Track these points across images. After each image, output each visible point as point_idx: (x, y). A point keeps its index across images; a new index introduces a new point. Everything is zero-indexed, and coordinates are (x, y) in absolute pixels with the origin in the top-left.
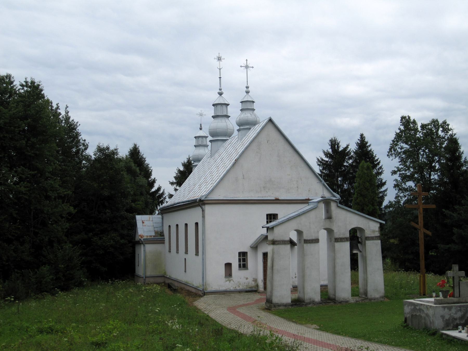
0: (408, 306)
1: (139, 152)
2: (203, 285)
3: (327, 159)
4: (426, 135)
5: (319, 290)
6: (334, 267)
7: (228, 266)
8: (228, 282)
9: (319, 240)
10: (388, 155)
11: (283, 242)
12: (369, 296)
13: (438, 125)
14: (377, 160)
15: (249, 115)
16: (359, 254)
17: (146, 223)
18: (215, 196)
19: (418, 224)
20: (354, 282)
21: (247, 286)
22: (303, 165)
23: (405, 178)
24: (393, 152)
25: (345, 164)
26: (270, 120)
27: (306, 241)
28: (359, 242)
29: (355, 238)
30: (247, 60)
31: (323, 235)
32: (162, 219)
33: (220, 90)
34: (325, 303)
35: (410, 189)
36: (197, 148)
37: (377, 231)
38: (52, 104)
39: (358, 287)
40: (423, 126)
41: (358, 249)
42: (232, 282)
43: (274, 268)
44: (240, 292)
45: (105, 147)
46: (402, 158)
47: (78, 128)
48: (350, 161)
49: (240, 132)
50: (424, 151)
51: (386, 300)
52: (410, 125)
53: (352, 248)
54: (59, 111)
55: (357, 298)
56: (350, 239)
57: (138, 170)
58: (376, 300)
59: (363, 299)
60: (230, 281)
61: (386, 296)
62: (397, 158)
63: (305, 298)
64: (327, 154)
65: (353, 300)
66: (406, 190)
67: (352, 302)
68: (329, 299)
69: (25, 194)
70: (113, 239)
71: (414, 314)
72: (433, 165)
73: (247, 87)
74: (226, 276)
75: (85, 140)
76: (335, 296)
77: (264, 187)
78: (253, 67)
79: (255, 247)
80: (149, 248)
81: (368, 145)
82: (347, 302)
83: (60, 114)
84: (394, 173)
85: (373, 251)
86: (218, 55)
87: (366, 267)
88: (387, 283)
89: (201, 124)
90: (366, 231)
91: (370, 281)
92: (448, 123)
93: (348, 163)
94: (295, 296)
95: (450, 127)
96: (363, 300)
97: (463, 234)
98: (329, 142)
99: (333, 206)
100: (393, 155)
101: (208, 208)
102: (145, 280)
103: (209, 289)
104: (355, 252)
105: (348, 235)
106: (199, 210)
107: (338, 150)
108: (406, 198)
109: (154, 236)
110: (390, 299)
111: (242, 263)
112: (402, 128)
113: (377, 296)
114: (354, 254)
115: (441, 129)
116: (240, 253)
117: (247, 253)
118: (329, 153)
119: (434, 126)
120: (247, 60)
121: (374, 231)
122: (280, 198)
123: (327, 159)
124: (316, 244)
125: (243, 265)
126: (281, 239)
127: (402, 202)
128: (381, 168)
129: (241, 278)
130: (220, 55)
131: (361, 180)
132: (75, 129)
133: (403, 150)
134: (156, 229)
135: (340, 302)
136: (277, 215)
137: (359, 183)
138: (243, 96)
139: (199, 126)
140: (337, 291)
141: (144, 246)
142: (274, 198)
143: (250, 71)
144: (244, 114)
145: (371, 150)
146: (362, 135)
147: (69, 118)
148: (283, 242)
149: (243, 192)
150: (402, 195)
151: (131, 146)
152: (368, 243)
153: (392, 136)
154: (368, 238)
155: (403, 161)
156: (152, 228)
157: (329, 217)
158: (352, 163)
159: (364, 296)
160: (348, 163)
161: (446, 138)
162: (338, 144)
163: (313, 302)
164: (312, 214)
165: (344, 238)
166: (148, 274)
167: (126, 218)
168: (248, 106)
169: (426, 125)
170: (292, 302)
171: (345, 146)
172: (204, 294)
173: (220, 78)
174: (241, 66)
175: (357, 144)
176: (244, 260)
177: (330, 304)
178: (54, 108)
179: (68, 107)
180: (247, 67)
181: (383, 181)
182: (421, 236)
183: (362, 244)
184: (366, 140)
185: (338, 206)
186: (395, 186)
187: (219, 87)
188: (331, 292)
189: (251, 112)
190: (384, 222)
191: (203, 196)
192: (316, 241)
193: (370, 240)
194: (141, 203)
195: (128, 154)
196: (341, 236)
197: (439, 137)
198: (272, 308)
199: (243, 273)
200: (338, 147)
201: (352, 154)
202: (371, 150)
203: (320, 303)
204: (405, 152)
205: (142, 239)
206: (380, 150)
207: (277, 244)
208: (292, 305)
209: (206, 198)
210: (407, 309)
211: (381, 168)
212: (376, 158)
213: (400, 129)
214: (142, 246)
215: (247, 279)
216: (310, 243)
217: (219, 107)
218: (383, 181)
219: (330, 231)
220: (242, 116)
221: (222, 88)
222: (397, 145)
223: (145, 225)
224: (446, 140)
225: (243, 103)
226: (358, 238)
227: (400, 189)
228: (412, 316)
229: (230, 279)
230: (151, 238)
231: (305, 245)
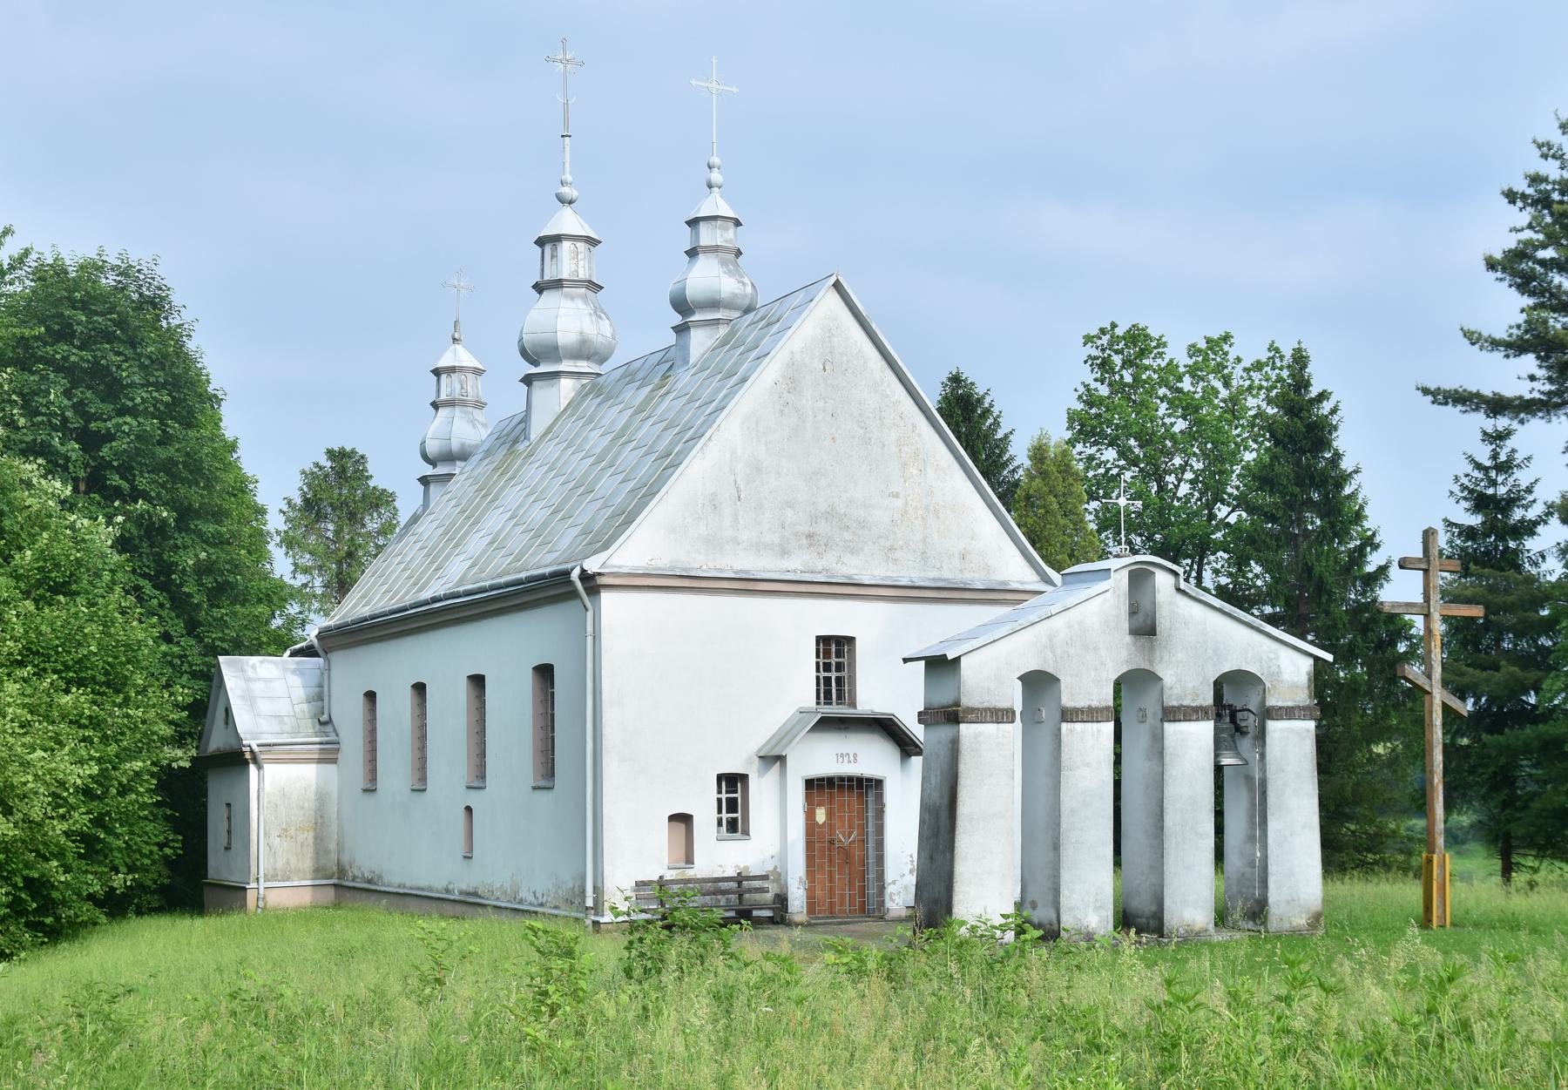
29: (1235, 709)
69: (831, 879)
105: (1208, 699)
125: (734, 821)
126: (986, 705)
136: (850, 640)
140: (1167, 903)
141: (260, 768)
182: (1437, 702)
190: (1329, 657)
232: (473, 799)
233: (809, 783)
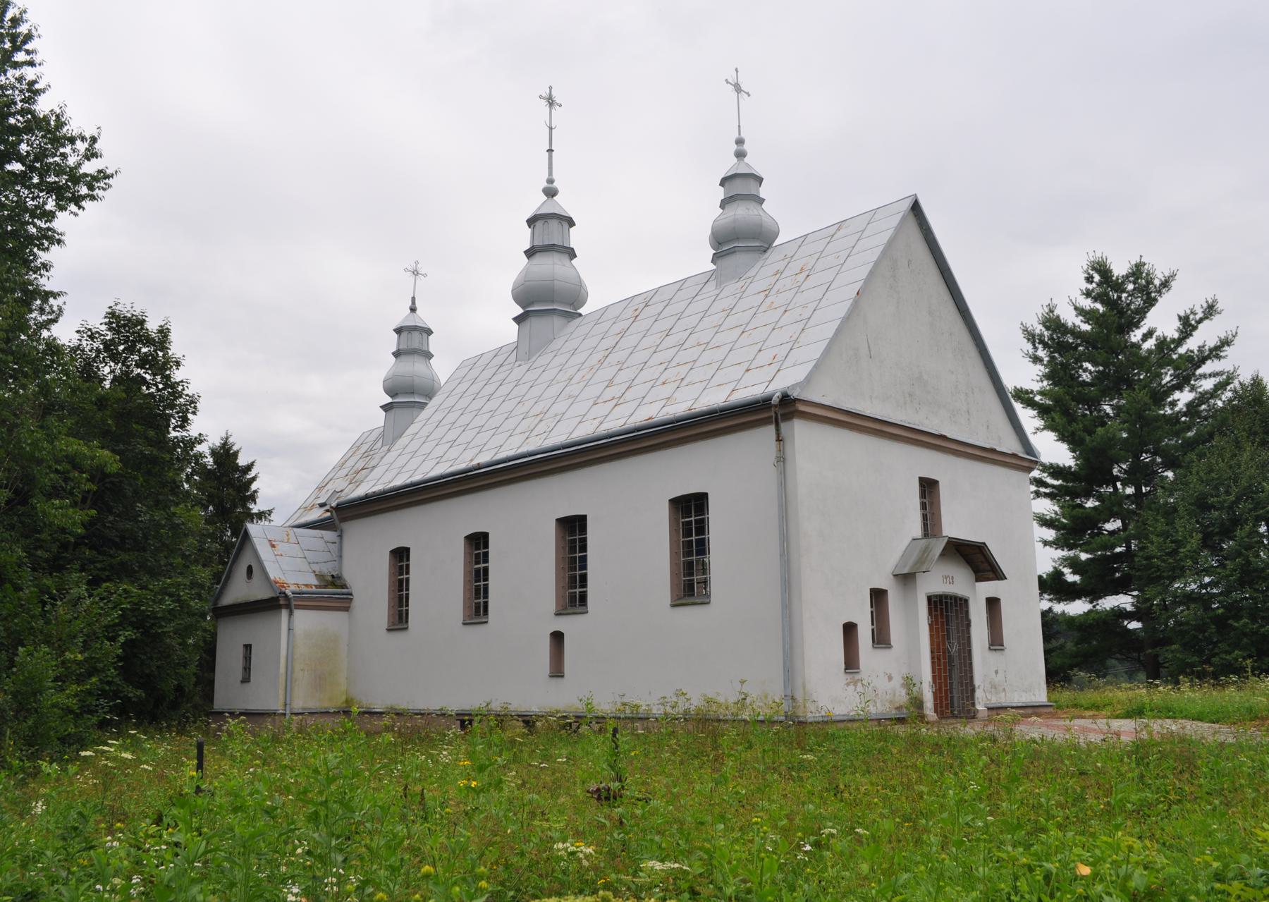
3: (1086, 327)
18: (824, 394)
33: (550, 181)
73: (740, 142)
77: (910, 395)
79: (906, 579)
80: (305, 621)
89: (413, 299)
101: (799, 430)
106: (761, 439)
123: (1086, 327)
134: (316, 568)
141: (291, 614)
166: (299, 703)
173: (550, 151)
187: (546, 176)
189: (565, 258)
199: (882, 654)
214: (284, 613)
221: (555, 176)
232: (566, 625)
233: (929, 599)
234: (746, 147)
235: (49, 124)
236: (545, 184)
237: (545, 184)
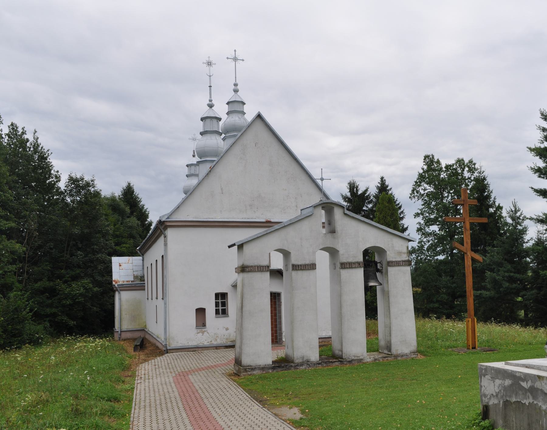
0: (493, 379)
1: (133, 192)
2: (166, 339)
3: (345, 204)
4: (450, 176)
5: (316, 343)
6: (340, 307)
7: (201, 312)
8: (201, 334)
9: (315, 265)
10: (410, 197)
11: (261, 269)
12: (394, 351)
13: (464, 164)
14: (399, 204)
15: (237, 118)
16: (378, 288)
17: (123, 266)
18: (181, 216)
19: (463, 245)
20: (371, 332)
21: (227, 339)
22: (304, 177)
23: (429, 222)
24: (416, 194)
25: (365, 208)
26: (259, 116)
27: (296, 267)
28: (378, 270)
29: (372, 264)
30: (235, 51)
31: (323, 260)
32: (143, 260)
33: (211, 101)
34: (326, 363)
35: (434, 234)
36: (190, 178)
37: (404, 253)
38: (17, 128)
39: (377, 339)
40: (447, 167)
41: (376, 279)
42: (205, 333)
43: (244, 309)
44: (217, 347)
45: (78, 177)
46: (425, 200)
47: (49, 157)
48: (370, 206)
49: (226, 141)
50: (449, 192)
51: (420, 357)
52: (433, 165)
53: (367, 278)
54: (26, 137)
55: (376, 355)
56: (365, 265)
57: (128, 210)
58: (404, 357)
59: (385, 355)
60: (203, 333)
61: (418, 352)
62: (420, 200)
63: (295, 356)
64: (345, 198)
65: (368, 358)
66: (429, 234)
67: (369, 360)
68: (334, 356)
70: (84, 287)
71: (514, 400)
72: (458, 207)
73: (236, 85)
74: (197, 326)
75: (58, 172)
76: (342, 351)
77: (250, 205)
78: (243, 60)
81: (388, 188)
82: (360, 361)
83: (28, 140)
84: (417, 215)
85: (400, 288)
86: (207, 59)
87: (389, 307)
88: (418, 330)
90: (388, 253)
91: (394, 328)
92: (474, 162)
93: (367, 207)
94: (281, 353)
95: (476, 166)
96: (385, 357)
97: (497, 278)
98: (347, 185)
99: (338, 213)
100: (416, 197)
102: (120, 335)
103: (174, 345)
104: (371, 284)
105: (360, 258)
107: (357, 193)
108: (429, 243)
109: (132, 281)
110: (425, 355)
111: (220, 308)
112: (425, 167)
113: (406, 350)
114: (371, 287)
115: (467, 169)
116: (217, 295)
117: (227, 293)
118: (347, 198)
119: (460, 166)
120: (235, 51)
121: (400, 253)
122: (272, 220)
124: (311, 272)
126: (256, 264)
127: (426, 247)
128: (402, 212)
129: (219, 328)
130: (211, 59)
131: (381, 214)
132: (46, 158)
133: (426, 192)
134: (136, 273)
135: (350, 362)
137: (379, 218)
138: (230, 96)
139: (192, 153)
142: (264, 220)
143: (239, 64)
144: (230, 117)
145: (391, 194)
146: (382, 178)
147: (38, 146)
148: (261, 269)
149: (221, 211)
150: (425, 240)
151: (125, 185)
152: (392, 271)
153: (415, 177)
154: (391, 264)
155: (427, 204)
156: (130, 273)
157: (331, 228)
158: (372, 207)
159: (386, 352)
160: (367, 207)
161: (472, 178)
162: (357, 187)
163: (308, 363)
164: (305, 225)
165: (354, 263)
166: (124, 328)
167: (104, 262)
168: (237, 107)
169: (450, 166)
170: (273, 362)
171: (364, 189)
172: (167, 351)
173: (210, 86)
174: (228, 58)
175: (378, 187)
176: (224, 304)
177: (334, 364)
178: (20, 133)
179: (36, 132)
180: (235, 59)
181: (405, 226)
183: (382, 273)
184: (387, 183)
185: (345, 214)
186: (419, 230)
187: (209, 98)
188: (336, 346)
189: (240, 115)
191: (163, 216)
192: (312, 267)
193: (395, 266)
194: (128, 245)
195: (120, 193)
196: (351, 260)
197: (464, 179)
198: (240, 372)
199: (222, 321)
200: (357, 190)
201: (372, 198)
202: (391, 194)
203: (319, 364)
204: (428, 195)
205: (116, 285)
206: (401, 193)
207: (249, 272)
208: (273, 368)
209: (168, 218)
210: (490, 387)
211: (402, 212)
212: (397, 202)
213: (423, 169)
215: (227, 329)
216: (301, 269)
217: (208, 121)
218: (405, 226)
219: (333, 252)
220: (228, 119)
221: (212, 99)
222: (419, 186)
223: (122, 268)
224: (472, 181)
225: (230, 104)
226: (376, 263)
227: (423, 234)
228: (507, 403)
229: (204, 330)
230: (128, 283)
231: (294, 273)
234: (238, 87)
235: (49, 179)
236: (208, 102)
237: (208, 102)
